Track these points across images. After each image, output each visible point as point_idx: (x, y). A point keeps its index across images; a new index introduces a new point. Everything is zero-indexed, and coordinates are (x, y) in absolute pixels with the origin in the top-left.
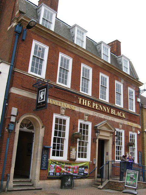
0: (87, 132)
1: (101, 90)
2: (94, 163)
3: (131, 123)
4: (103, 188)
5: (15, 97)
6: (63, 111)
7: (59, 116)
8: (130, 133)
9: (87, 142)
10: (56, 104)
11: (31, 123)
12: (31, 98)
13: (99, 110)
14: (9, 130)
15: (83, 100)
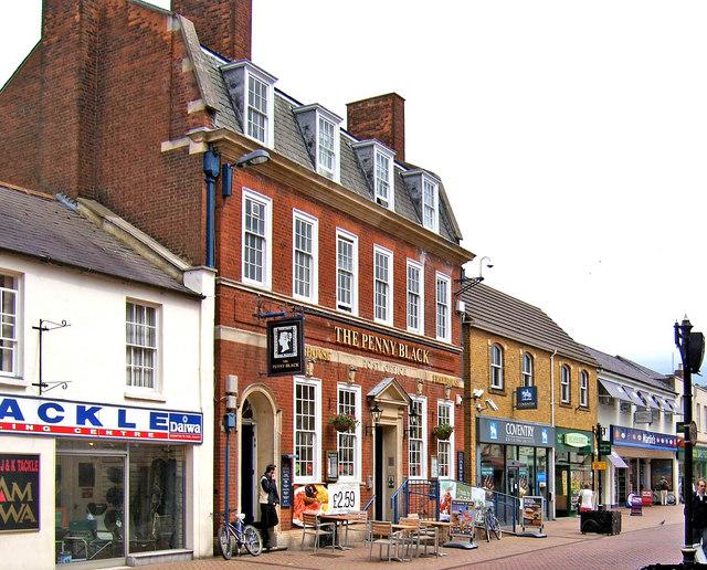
8: (440, 402)
13: (374, 353)
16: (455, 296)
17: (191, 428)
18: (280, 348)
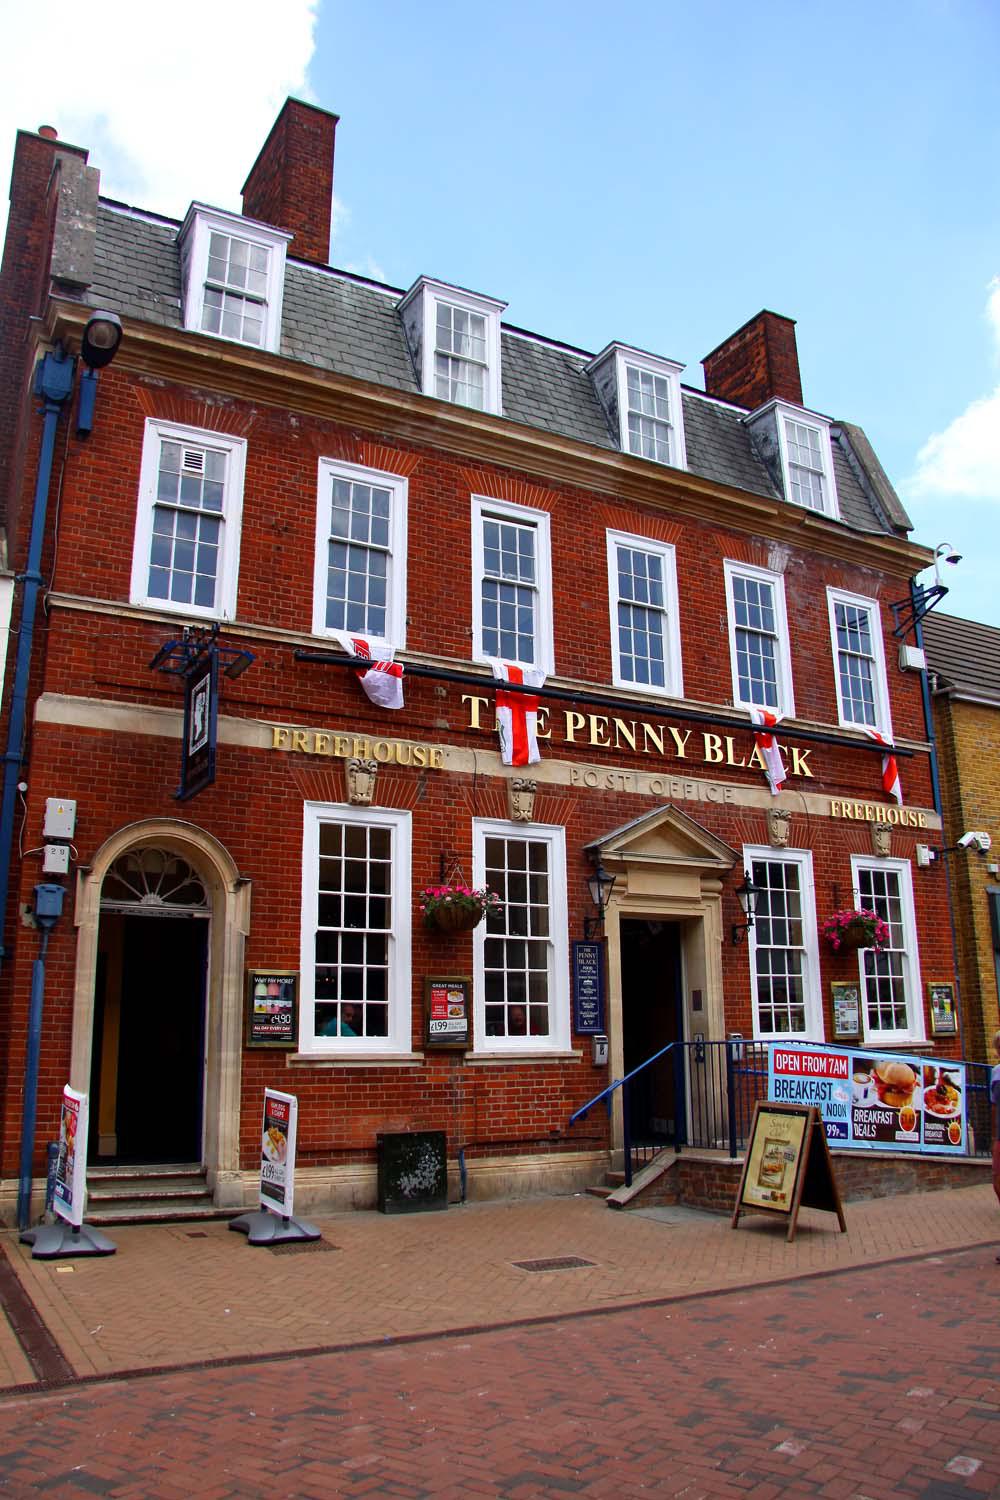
0: (896, 905)
1: (844, 679)
2: (600, 1059)
3: (857, 803)
4: (630, 1203)
5: (64, 745)
6: (362, 784)
7: (339, 814)
9: (900, 953)
10: (854, 814)
11: (183, 869)
12: (158, 738)
14: (39, 918)
15: (791, 752)
16: (893, 642)
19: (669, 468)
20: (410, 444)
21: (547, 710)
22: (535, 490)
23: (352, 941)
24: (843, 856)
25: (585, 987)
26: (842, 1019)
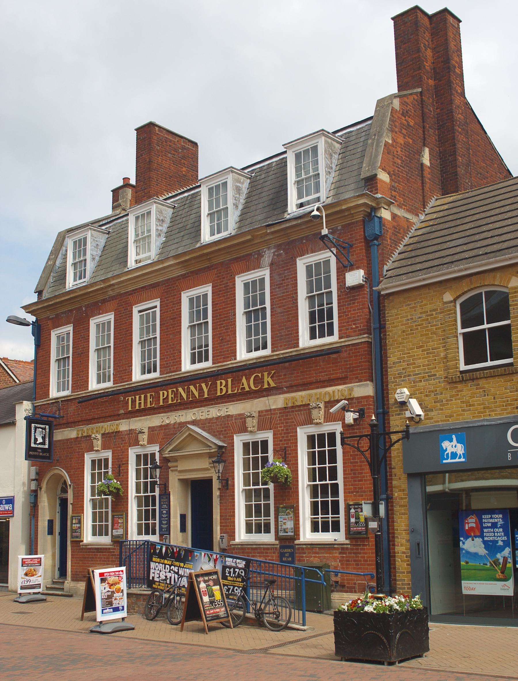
7: (247, 437)
17: (7, 507)
18: (36, 440)
19: (69, 291)
20: (114, 296)
21: (153, 394)
22: (235, 266)
23: (324, 487)
24: (293, 429)
25: (163, 514)
26: (284, 527)
